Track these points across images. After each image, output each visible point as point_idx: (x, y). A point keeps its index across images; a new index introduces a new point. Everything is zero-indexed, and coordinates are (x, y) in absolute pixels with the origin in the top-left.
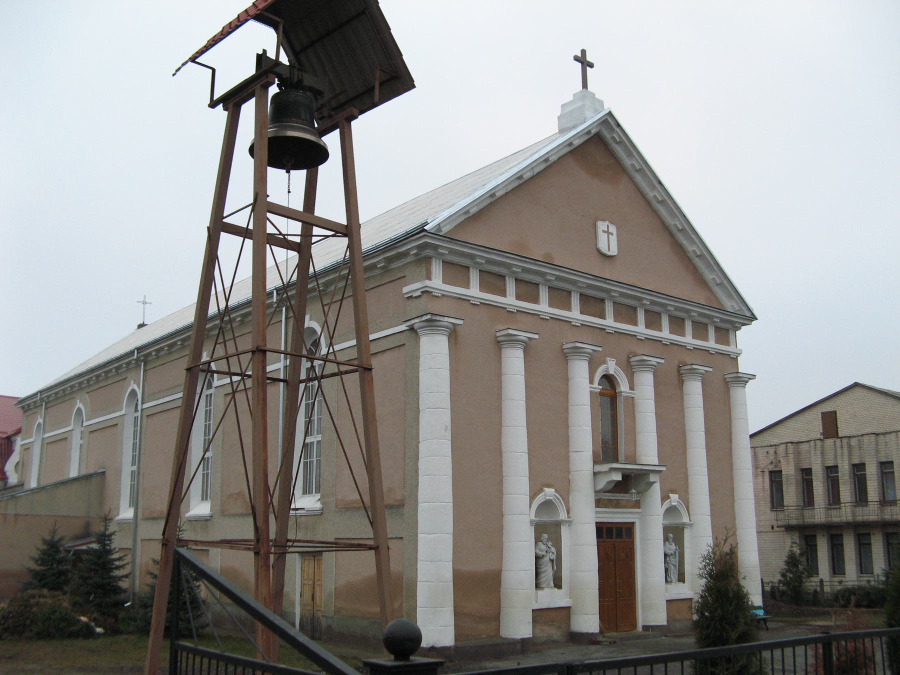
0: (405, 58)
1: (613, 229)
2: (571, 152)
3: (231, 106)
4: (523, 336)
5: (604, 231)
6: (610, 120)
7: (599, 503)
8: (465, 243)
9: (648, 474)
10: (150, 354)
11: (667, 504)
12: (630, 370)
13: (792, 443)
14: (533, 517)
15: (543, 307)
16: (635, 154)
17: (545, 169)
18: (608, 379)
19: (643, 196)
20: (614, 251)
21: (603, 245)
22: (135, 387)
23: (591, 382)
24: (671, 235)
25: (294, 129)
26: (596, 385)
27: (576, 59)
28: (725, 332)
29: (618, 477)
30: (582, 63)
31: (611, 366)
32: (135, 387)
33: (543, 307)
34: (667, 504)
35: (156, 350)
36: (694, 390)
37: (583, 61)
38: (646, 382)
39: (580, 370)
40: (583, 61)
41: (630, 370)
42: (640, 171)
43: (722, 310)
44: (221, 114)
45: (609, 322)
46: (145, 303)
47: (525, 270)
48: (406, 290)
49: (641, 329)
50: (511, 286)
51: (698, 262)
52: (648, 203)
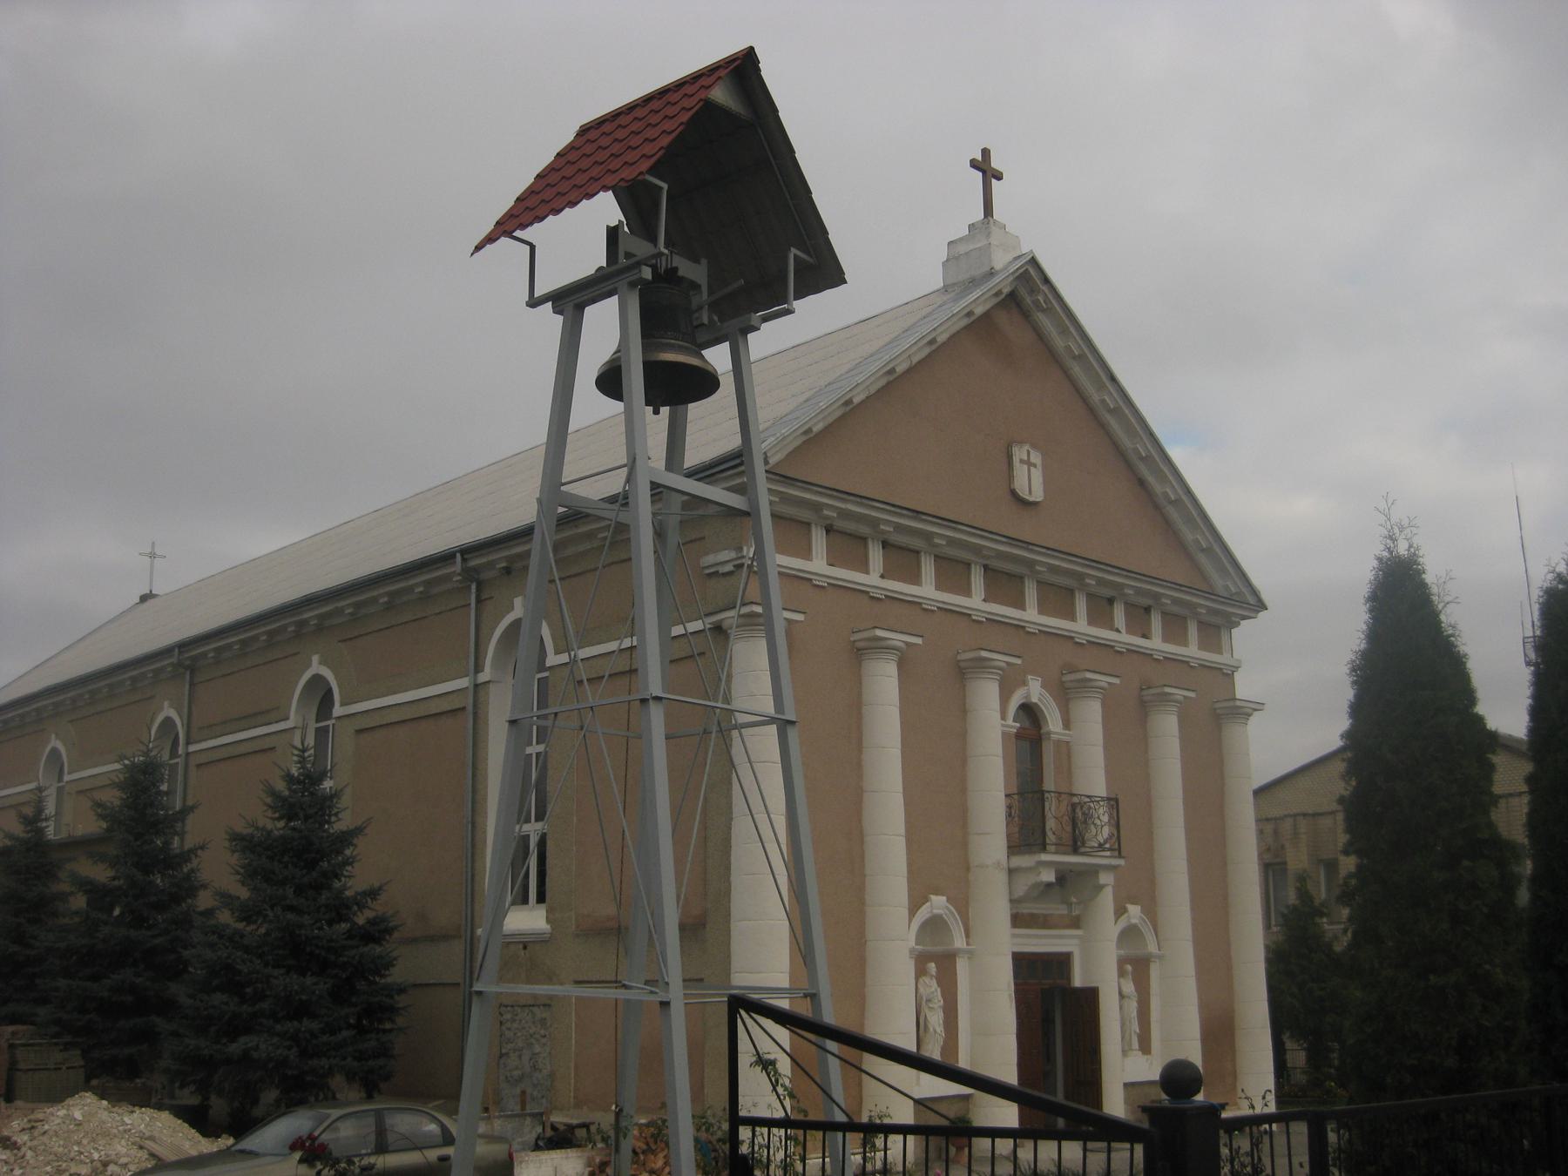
0: (833, 238)
1: (1036, 458)
2: (967, 328)
3: (569, 308)
4: (898, 639)
5: (1022, 461)
6: (1032, 271)
7: (1018, 920)
8: (807, 485)
9: (1097, 872)
10: (204, 655)
11: (1123, 922)
12: (1065, 694)
13: (1305, 815)
14: (912, 943)
15: (927, 590)
16: (1072, 329)
17: (929, 356)
18: (1029, 711)
19: (1085, 400)
20: (1038, 495)
21: (1020, 485)
22: (173, 714)
23: (1003, 717)
24: (1129, 465)
25: (671, 348)
26: (1010, 721)
27: (974, 164)
28: (1215, 629)
29: (1049, 876)
30: (984, 172)
31: (1035, 690)
32: (173, 714)
33: (927, 590)
34: (1123, 922)
35: (215, 650)
36: (1167, 728)
37: (985, 168)
38: (1091, 713)
39: (986, 693)
40: (985, 168)
41: (1065, 694)
42: (1080, 358)
43: (1211, 594)
44: (550, 322)
45: (1031, 614)
46: (152, 556)
47: (899, 528)
48: (710, 559)
49: (1081, 626)
50: (928, 568)
51: (1172, 512)
52: (1091, 410)
